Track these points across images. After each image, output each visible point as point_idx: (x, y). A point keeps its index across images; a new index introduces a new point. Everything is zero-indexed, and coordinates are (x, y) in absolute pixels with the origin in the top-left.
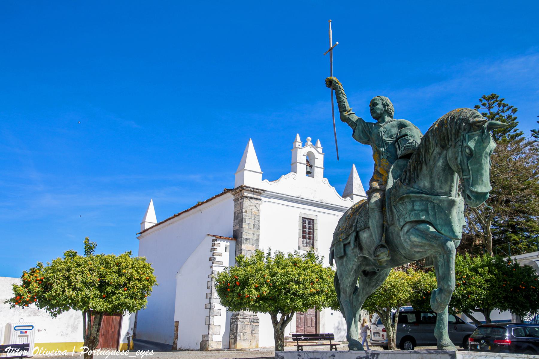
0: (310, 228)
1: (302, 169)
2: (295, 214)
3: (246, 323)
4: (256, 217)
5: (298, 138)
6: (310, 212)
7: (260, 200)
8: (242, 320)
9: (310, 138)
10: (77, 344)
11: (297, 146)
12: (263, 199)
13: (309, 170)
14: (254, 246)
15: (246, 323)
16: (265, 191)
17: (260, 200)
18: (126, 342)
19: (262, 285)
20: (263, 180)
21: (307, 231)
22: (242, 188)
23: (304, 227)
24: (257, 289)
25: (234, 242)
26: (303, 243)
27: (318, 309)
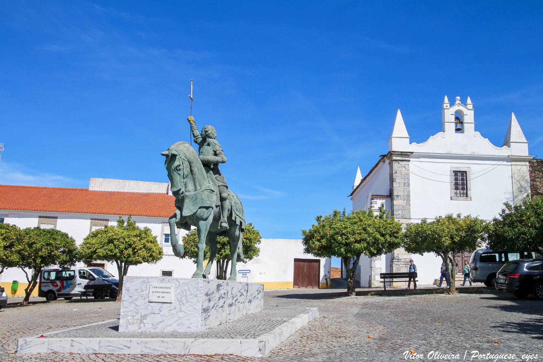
0: (463, 179)
1: (450, 127)
2: (444, 170)
3: (401, 266)
4: (407, 177)
5: (446, 100)
6: (461, 165)
7: (409, 161)
8: (397, 263)
9: (458, 98)
10: (287, 283)
11: (445, 107)
12: (411, 159)
13: (459, 126)
14: (405, 201)
15: (401, 266)
16: (412, 153)
17: (409, 161)
18: (325, 281)
19: (322, 237)
20: (410, 143)
21: (460, 182)
22: (391, 154)
23: (456, 179)
24: (319, 240)
25: (389, 199)
26: (456, 193)
27: (358, 256)
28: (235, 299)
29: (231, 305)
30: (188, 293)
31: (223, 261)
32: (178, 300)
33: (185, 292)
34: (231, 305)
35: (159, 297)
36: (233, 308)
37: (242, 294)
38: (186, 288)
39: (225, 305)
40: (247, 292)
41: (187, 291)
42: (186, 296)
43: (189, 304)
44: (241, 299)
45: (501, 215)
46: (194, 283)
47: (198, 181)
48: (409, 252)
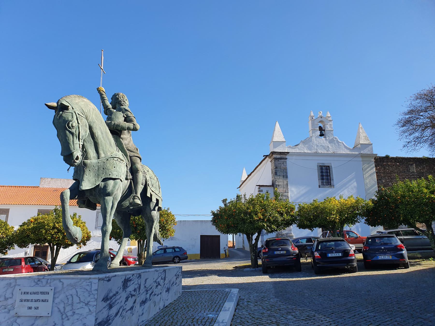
6: (326, 161)
16: (288, 153)
23: (322, 172)
28: (150, 292)
29: (143, 302)
30: (76, 300)
31: (144, 241)
32: (60, 311)
33: (70, 299)
34: (143, 302)
35: (30, 308)
36: (147, 305)
37: (159, 284)
38: (73, 292)
39: (135, 304)
40: (165, 280)
41: (75, 297)
42: (72, 304)
43: (76, 317)
44: (157, 291)
45: (376, 196)
46: (84, 283)
47: (103, 151)
48: (300, 228)
